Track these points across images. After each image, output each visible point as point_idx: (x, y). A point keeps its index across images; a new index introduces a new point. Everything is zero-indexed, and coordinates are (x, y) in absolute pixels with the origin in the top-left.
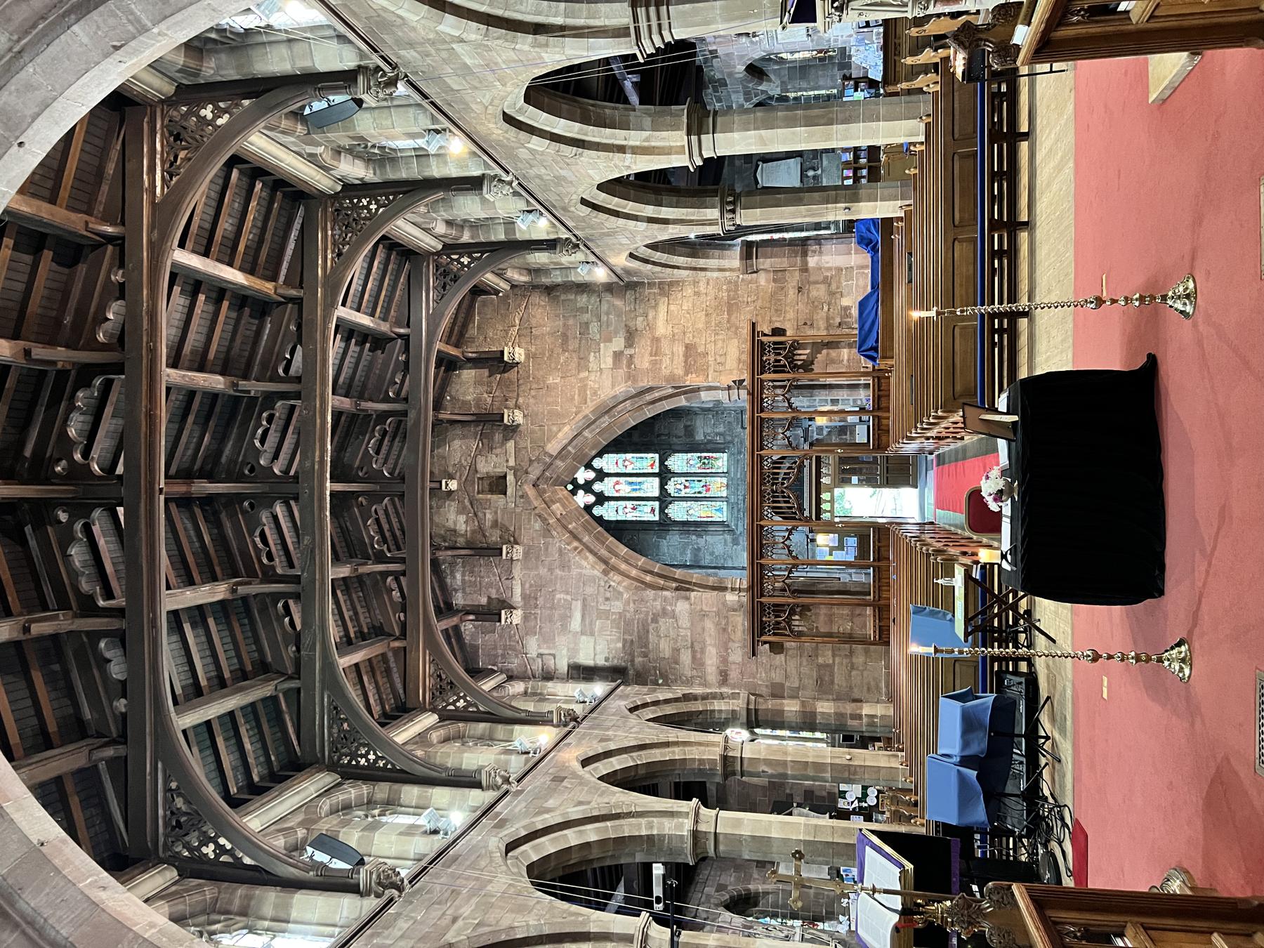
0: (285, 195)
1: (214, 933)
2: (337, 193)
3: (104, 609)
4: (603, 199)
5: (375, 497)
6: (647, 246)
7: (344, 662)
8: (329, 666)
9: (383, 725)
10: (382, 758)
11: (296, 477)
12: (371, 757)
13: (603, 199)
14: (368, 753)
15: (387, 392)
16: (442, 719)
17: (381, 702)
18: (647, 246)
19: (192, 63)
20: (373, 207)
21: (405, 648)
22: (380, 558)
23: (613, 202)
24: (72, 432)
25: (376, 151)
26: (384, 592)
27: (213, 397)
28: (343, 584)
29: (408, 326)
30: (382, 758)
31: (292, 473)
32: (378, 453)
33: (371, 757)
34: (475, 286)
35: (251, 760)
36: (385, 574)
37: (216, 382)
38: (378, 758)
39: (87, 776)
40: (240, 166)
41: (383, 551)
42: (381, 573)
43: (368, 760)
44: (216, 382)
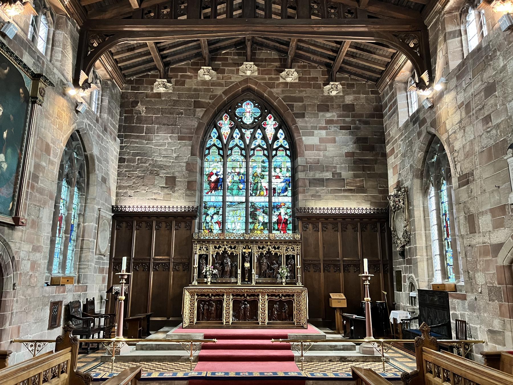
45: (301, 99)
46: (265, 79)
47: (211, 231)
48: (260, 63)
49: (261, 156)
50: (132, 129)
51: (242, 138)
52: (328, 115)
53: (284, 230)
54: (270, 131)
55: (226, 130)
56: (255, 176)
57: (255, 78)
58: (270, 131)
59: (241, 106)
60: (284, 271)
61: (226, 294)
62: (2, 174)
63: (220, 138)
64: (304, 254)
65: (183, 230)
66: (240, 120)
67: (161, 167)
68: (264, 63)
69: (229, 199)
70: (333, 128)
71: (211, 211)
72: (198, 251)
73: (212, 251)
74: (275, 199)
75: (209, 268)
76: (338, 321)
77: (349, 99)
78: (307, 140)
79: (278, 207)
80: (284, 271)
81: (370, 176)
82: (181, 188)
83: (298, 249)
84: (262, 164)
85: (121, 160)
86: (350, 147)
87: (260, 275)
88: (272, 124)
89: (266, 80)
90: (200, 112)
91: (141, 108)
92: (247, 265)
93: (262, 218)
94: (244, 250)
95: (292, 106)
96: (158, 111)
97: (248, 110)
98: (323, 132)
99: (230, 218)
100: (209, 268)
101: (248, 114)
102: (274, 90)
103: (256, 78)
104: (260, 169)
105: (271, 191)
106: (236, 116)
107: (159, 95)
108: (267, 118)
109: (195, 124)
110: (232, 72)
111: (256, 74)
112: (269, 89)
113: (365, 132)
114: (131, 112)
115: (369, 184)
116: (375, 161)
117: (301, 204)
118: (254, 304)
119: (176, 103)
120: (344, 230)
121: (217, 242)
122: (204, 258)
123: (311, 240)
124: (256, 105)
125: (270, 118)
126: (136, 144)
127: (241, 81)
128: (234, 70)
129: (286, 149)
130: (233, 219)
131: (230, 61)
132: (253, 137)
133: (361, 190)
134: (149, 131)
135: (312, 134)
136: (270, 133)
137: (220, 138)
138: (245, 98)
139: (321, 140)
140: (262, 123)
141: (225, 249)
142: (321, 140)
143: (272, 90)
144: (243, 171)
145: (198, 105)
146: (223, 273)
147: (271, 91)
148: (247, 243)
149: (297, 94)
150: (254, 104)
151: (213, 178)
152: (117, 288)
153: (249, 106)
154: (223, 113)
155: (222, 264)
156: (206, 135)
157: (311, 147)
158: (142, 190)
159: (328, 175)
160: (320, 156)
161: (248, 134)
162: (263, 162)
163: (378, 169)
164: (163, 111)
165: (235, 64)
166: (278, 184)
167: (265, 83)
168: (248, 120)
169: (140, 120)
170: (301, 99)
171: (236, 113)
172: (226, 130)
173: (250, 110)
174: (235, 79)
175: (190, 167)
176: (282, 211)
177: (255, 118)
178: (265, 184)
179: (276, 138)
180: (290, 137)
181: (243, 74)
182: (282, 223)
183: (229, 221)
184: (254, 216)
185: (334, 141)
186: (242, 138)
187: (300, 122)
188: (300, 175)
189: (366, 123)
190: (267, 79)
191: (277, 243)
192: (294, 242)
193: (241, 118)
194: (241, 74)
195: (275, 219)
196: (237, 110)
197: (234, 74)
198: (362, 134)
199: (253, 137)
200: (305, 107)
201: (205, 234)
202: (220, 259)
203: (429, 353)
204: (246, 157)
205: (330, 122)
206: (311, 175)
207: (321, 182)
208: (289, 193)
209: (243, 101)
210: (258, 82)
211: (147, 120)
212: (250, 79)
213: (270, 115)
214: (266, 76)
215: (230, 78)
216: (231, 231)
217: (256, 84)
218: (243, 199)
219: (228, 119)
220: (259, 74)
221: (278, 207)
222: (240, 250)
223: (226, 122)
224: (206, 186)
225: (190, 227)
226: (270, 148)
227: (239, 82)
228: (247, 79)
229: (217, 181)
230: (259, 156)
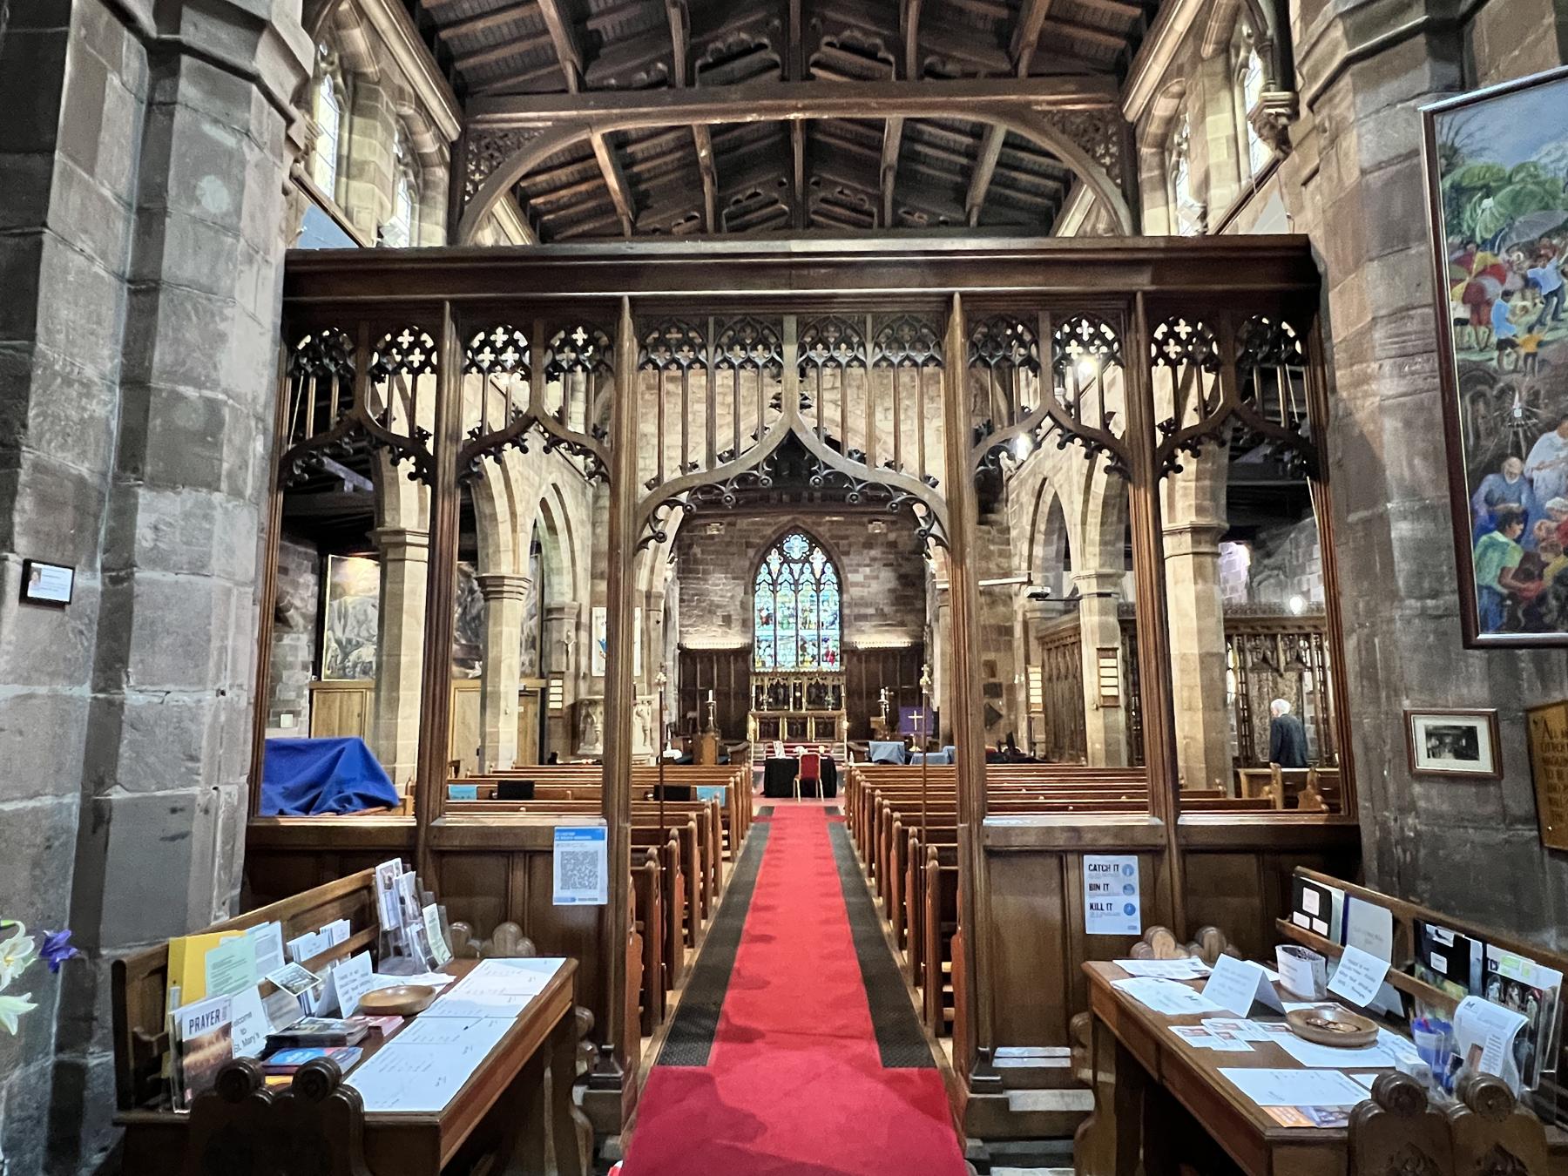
0: (1057, 191)
1: (334, 78)
2: (1123, 116)
3: (693, 66)
4: (1047, 498)
5: (790, 198)
6: (1056, 495)
7: (597, 141)
8: (588, 124)
9: (514, 189)
10: (476, 189)
11: (812, 77)
12: (477, 177)
13: (1047, 498)
14: (481, 172)
15: (932, 52)
16: (453, 146)
17: (556, 207)
18: (1056, 495)
19: (1150, 140)
20: (1107, 160)
21: (565, 91)
22: (719, 204)
23: (1045, 508)
24: (847, 33)
25: (1174, 158)
26: (647, 58)
27: (878, 147)
28: (686, 142)
29: (1030, 75)
30: (476, 189)
31: (814, 70)
32: (844, 47)
33: (477, 177)
34: (1075, 176)
35: (562, 213)
36: (669, 58)
37: (891, 153)
38: (476, 185)
39: (610, 209)
40: (1144, 20)
41: (703, 54)
42: (671, 54)
43: (473, 173)
44: (891, 153)
45: (846, 537)
47: (764, 663)
50: (690, 572)
51: (791, 573)
52: (873, 553)
53: (832, 661)
54: (818, 566)
55: (775, 567)
56: (804, 611)
58: (818, 566)
60: (830, 698)
61: (803, 327)
63: (770, 573)
64: (849, 682)
65: (740, 664)
67: (718, 606)
69: (780, 632)
70: (876, 565)
71: (763, 645)
72: (754, 683)
73: (767, 683)
74: (823, 633)
75: (764, 697)
76: (1465, 427)
77: (892, 536)
78: (852, 577)
79: (826, 641)
80: (830, 698)
81: (910, 611)
82: (736, 626)
83: (843, 679)
85: (682, 600)
86: (893, 584)
87: (809, 702)
90: (751, 552)
91: (697, 550)
93: (812, 650)
95: (837, 545)
96: (713, 553)
98: (868, 570)
100: (764, 697)
102: (821, 529)
105: (819, 625)
107: (712, 537)
109: (747, 563)
113: (907, 568)
114: (687, 554)
115: (909, 618)
116: (916, 597)
117: (846, 639)
118: (804, 726)
119: (728, 544)
120: (885, 662)
121: (774, 674)
122: (760, 689)
123: (856, 671)
126: (694, 586)
132: (802, 572)
133: (902, 624)
134: (705, 572)
135: (857, 571)
137: (770, 573)
139: (866, 577)
142: (866, 577)
144: (793, 605)
145: (748, 545)
146: (776, 700)
148: (797, 674)
149: (843, 533)
151: (764, 614)
152: (690, 715)
155: (776, 694)
156: (757, 572)
157: (856, 584)
158: (703, 628)
159: (871, 611)
160: (864, 592)
161: (796, 568)
163: (918, 605)
164: (717, 552)
166: (826, 617)
168: (796, 555)
169: (696, 561)
170: (846, 537)
172: (775, 567)
175: (743, 605)
176: (830, 643)
178: (813, 617)
179: (823, 572)
180: (837, 572)
182: (831, 657)
184: (804, 649)
185: (877, 578)
186: (791, 573)
187: (845, 560)
188: (846, 611)
189: (908, 559)
191: (824, 675)
192: (840, 673)
195: (823, 651)
198: (903, 571)
199: (802, 572)
200: (850, 545)
201: (759, 668)
202: (774, 689)
204: (796, 592)
205: (874, 559)
206: (856, 611)
207: (865, 617)
208: (837, 626)
211: (702, 562)
218: (793, 633)
221: (826, 641)
222: (792, 681)
224: (757, 620)
225: (746, 661)
226: (818, 582)
229: (768, 616)
230: (808, 590)
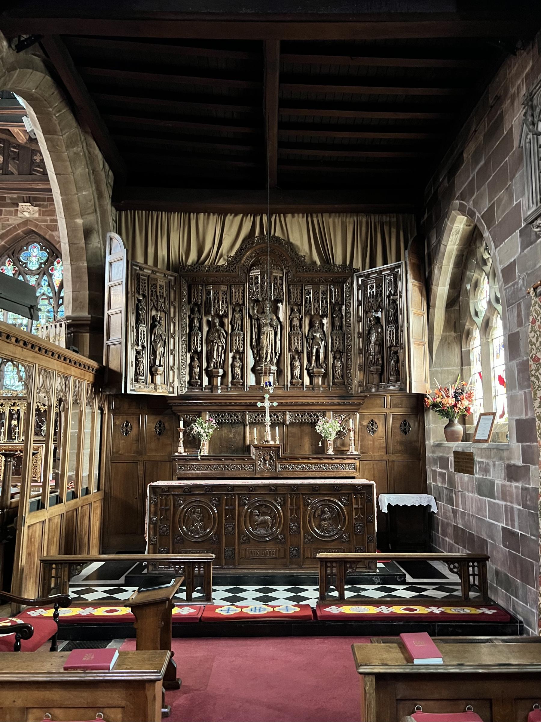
46: (46, 221)
48: (42, 203)
49: (46, 305)
57: (35, 220)
59: (27, 250)
62: (1, 321)
66: (43, 266)
68: (46, 203)
84: (47, 314)
88: (61, 269)
89: (47, 222)
92: (14, 422)
94: (12, 408)
97: (34, 254)
99: (8, 373)
101: (34, 259)
103: (36, 219)
104: (45, 320)
106: (20, 261)
108: (55, 263)
110: (10, 213)
111: (37, 215)
112: (50, 232)
124: (44, 248)
125: (58, 263)
127: (20, 224)
128: (12, 211)
129: (49, 298)
130: (12, 374)
131: (8, 201)
136: (58, 279)
138: (30, 240)
140: (50, 269)
141: (38, 406)
143: (54, 233)
147: (52, 235)
150: (41, 248)
153: (35, 250)
154: (4, 258)
162: (48, 311)
165: (14, 204)
167: (47, 226)
168: (33, 266)
171: (21, 258)
173: (36, 253)
174: (13, 221)
177: (41, 263)
181: (22, 216)
183: (8, 376)
190: (49, 221)
193: (26, 263)
194: (20, 215)
196: (22, 254)
197: (12, 215)
203: (330, 494)
209: (27, 245)
210: (38, 224)
212: (30, 221)
213: (58, 259)
214: (48, 218)
215: (8, 220)
216: (10, 387)
217: (36, 226)
219: (12, 264)
220: (40, 215)
223: (9, 268)
227: (18, 225)
228: (26, 222)
